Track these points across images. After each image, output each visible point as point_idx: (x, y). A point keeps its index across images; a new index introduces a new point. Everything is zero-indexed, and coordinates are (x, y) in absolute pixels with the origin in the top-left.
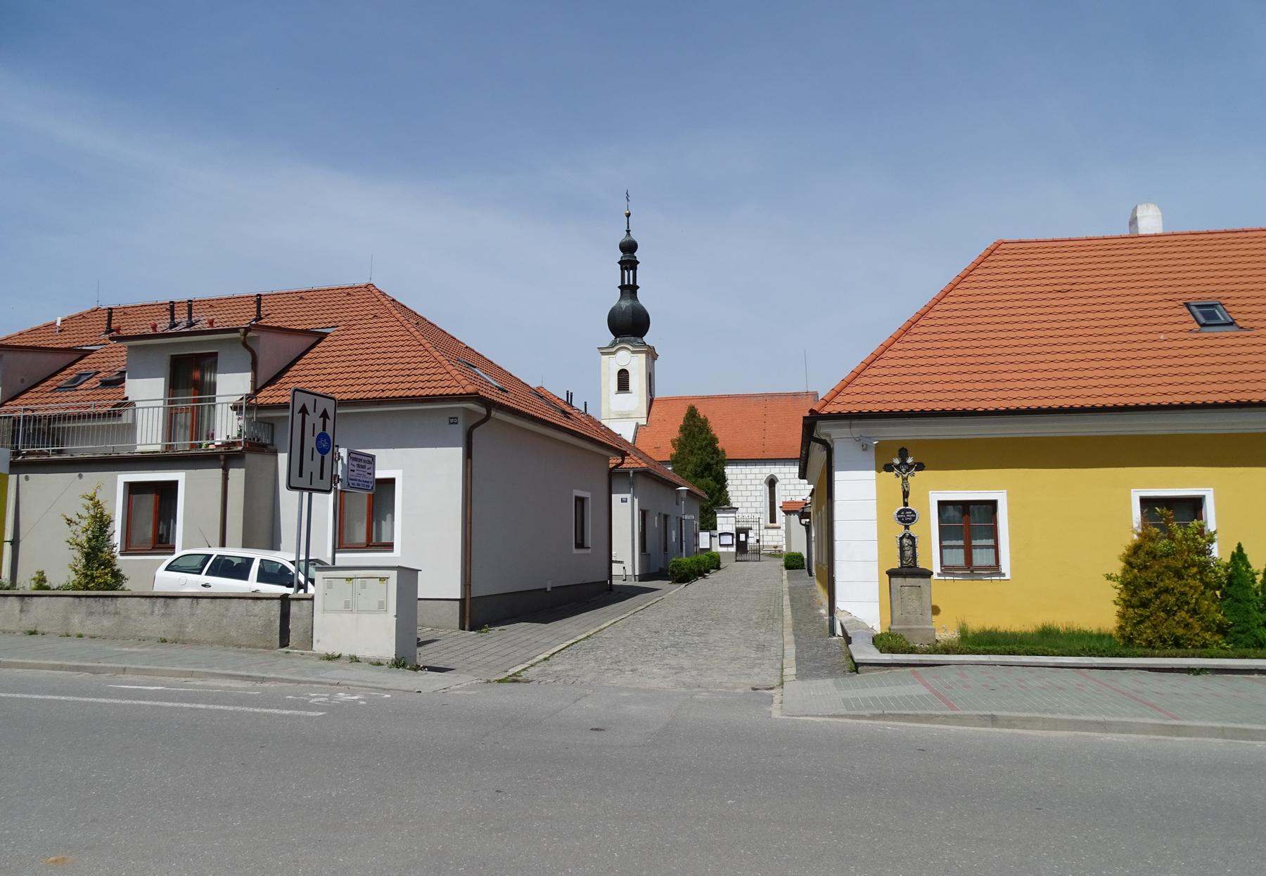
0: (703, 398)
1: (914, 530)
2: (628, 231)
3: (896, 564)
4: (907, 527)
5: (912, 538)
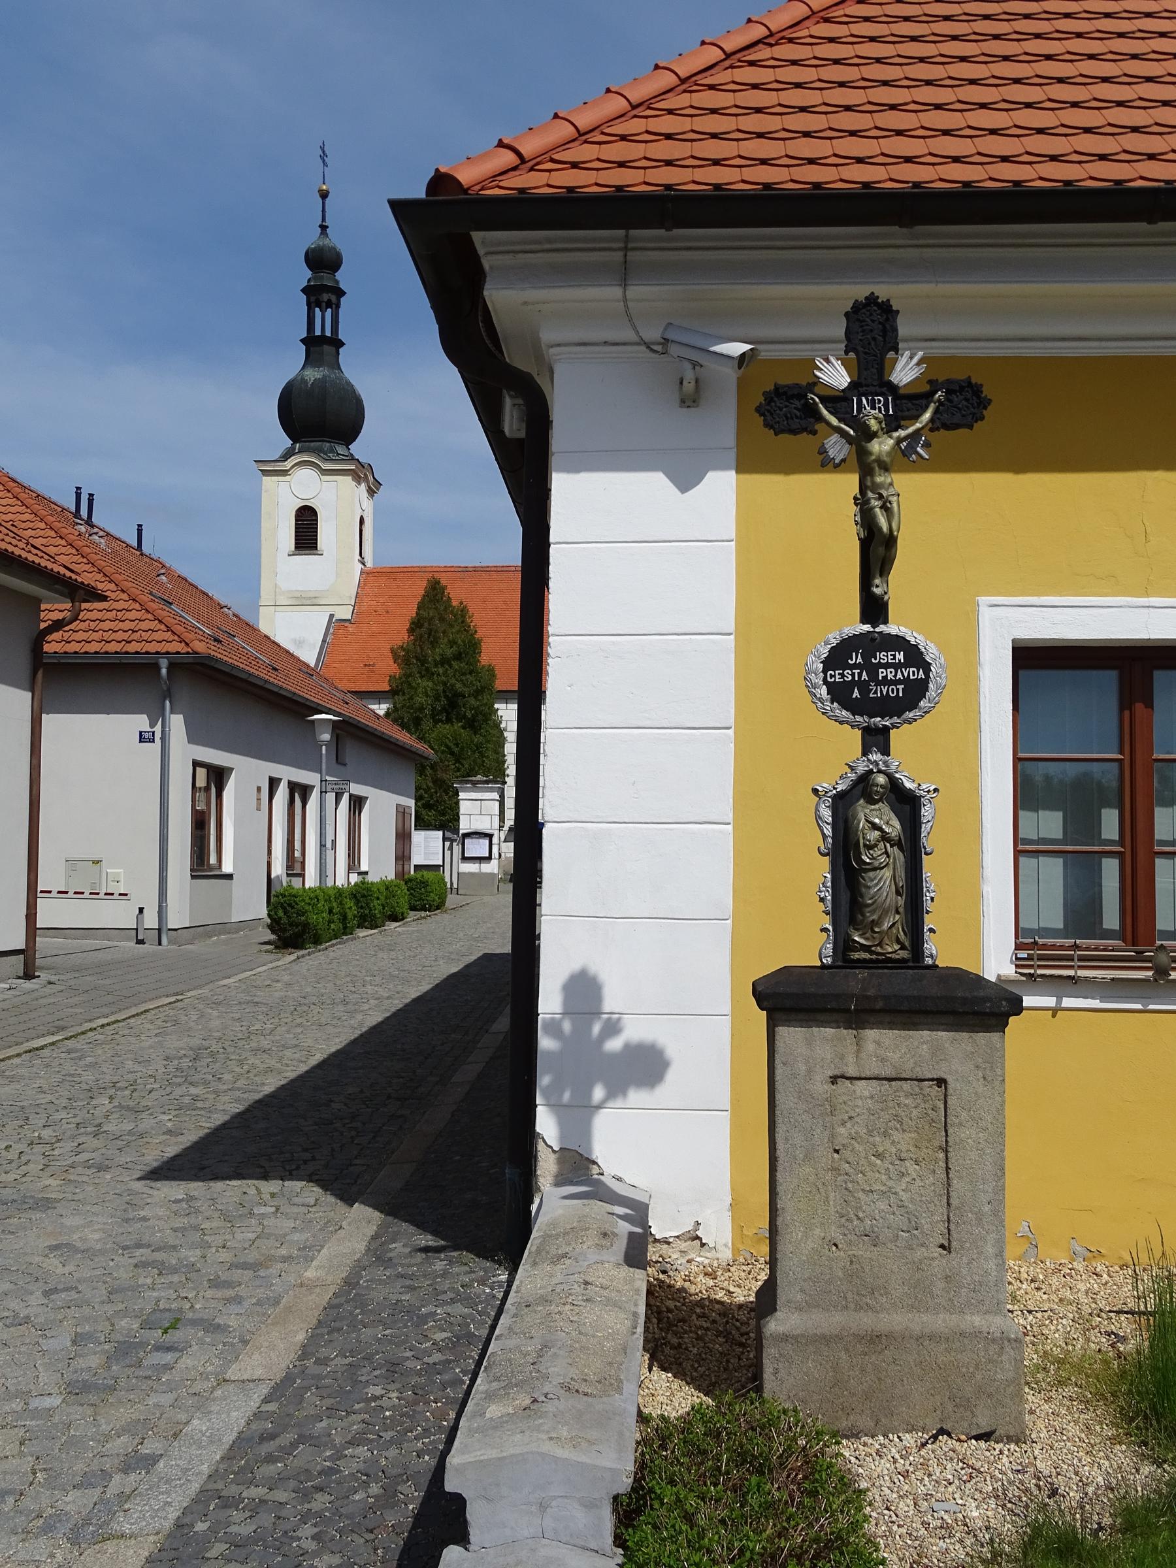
0: (465, 570)
1: (911, 754)
2: (324, 228)
3: (807, 943)
4: (876, 739)
5: (907, 803)
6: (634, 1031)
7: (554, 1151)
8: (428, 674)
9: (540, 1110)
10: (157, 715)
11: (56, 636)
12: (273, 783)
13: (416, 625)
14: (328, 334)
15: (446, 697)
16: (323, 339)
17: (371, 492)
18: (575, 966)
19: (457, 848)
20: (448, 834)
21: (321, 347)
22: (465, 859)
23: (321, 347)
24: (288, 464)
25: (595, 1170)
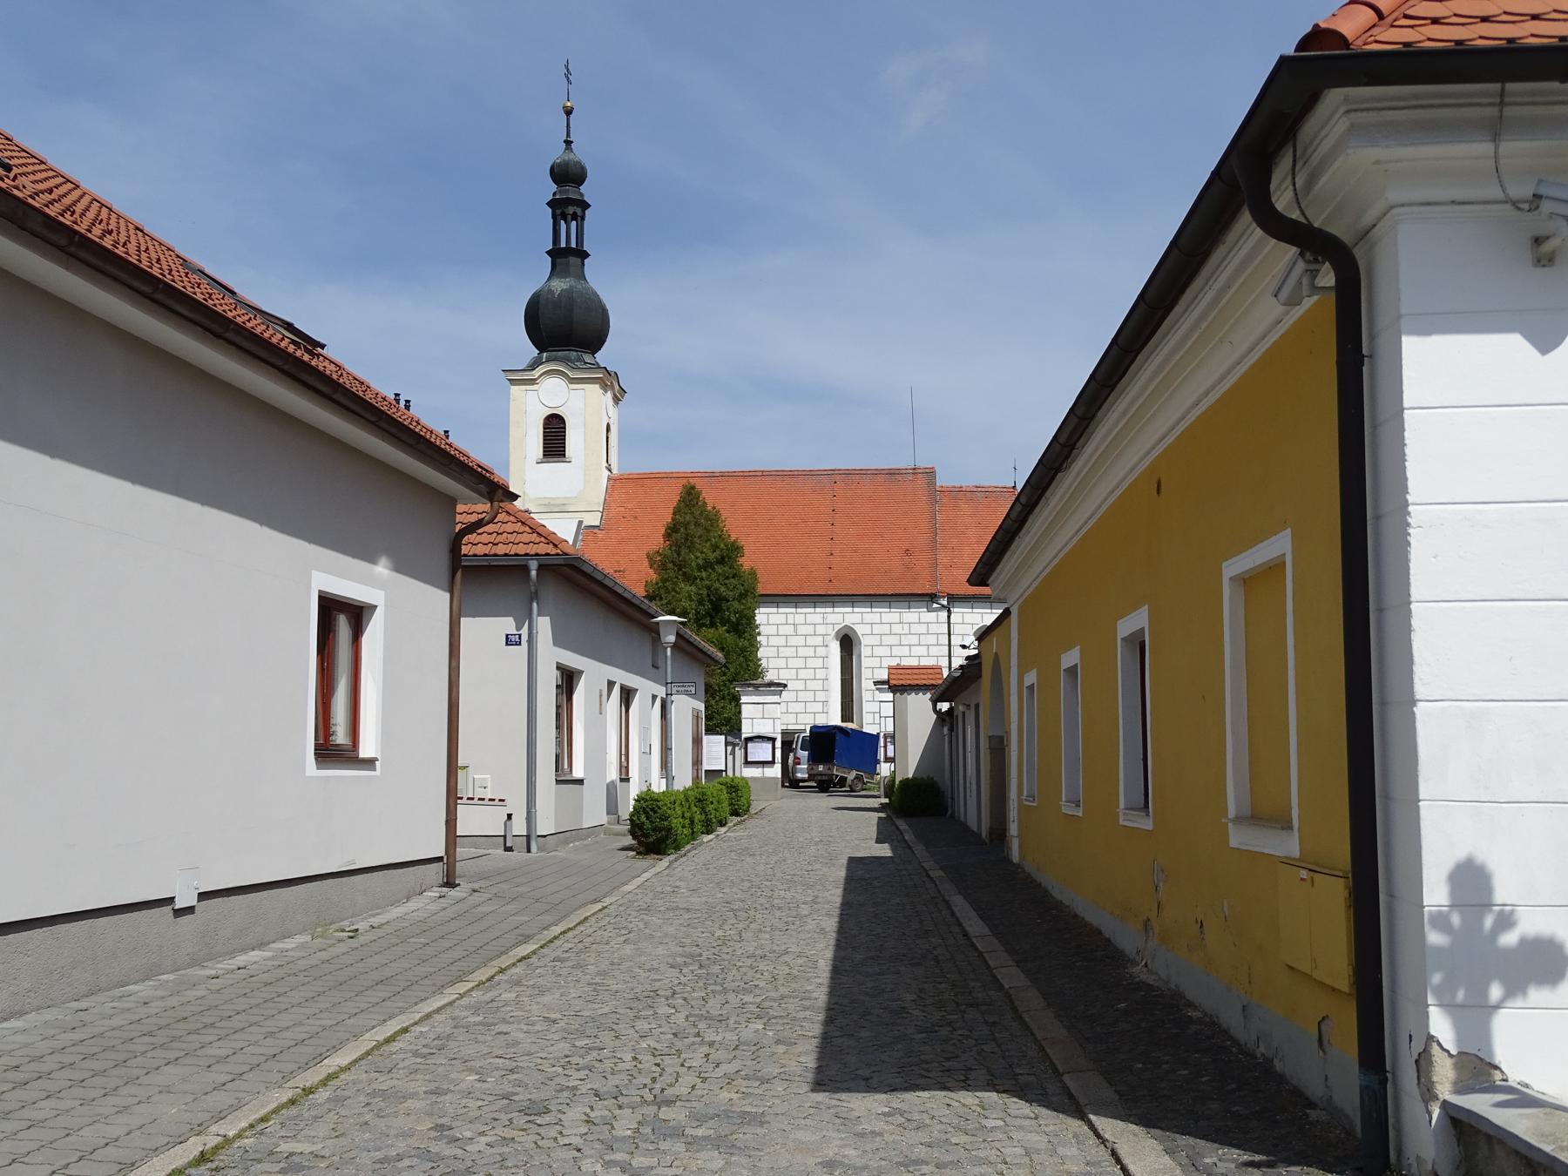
0: (712, 475)
2: (568, 143)
6: (1531, 924)
7: (1451, 1056)
8: (690, 579)
9: (1432, 1010)
10: (524, 617)
11: (472, 537)
12: (611, 684)
13: (671, 531)
14: (573, 245)
15: (710, 601)
16: (568, 251)
17: (617, 400)
18: (1460, 854)
19: (739, 753)
20: (730, 739)
21: (567, 257)
22: (747, 763)
23: (567, 257)
24: (536, 373)
25: (1497, 1076)
